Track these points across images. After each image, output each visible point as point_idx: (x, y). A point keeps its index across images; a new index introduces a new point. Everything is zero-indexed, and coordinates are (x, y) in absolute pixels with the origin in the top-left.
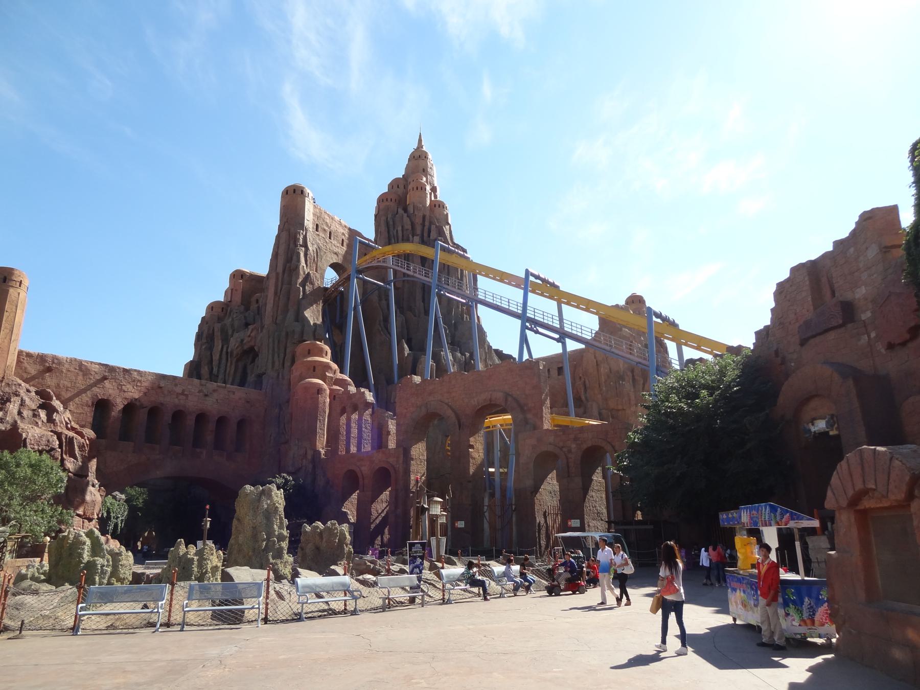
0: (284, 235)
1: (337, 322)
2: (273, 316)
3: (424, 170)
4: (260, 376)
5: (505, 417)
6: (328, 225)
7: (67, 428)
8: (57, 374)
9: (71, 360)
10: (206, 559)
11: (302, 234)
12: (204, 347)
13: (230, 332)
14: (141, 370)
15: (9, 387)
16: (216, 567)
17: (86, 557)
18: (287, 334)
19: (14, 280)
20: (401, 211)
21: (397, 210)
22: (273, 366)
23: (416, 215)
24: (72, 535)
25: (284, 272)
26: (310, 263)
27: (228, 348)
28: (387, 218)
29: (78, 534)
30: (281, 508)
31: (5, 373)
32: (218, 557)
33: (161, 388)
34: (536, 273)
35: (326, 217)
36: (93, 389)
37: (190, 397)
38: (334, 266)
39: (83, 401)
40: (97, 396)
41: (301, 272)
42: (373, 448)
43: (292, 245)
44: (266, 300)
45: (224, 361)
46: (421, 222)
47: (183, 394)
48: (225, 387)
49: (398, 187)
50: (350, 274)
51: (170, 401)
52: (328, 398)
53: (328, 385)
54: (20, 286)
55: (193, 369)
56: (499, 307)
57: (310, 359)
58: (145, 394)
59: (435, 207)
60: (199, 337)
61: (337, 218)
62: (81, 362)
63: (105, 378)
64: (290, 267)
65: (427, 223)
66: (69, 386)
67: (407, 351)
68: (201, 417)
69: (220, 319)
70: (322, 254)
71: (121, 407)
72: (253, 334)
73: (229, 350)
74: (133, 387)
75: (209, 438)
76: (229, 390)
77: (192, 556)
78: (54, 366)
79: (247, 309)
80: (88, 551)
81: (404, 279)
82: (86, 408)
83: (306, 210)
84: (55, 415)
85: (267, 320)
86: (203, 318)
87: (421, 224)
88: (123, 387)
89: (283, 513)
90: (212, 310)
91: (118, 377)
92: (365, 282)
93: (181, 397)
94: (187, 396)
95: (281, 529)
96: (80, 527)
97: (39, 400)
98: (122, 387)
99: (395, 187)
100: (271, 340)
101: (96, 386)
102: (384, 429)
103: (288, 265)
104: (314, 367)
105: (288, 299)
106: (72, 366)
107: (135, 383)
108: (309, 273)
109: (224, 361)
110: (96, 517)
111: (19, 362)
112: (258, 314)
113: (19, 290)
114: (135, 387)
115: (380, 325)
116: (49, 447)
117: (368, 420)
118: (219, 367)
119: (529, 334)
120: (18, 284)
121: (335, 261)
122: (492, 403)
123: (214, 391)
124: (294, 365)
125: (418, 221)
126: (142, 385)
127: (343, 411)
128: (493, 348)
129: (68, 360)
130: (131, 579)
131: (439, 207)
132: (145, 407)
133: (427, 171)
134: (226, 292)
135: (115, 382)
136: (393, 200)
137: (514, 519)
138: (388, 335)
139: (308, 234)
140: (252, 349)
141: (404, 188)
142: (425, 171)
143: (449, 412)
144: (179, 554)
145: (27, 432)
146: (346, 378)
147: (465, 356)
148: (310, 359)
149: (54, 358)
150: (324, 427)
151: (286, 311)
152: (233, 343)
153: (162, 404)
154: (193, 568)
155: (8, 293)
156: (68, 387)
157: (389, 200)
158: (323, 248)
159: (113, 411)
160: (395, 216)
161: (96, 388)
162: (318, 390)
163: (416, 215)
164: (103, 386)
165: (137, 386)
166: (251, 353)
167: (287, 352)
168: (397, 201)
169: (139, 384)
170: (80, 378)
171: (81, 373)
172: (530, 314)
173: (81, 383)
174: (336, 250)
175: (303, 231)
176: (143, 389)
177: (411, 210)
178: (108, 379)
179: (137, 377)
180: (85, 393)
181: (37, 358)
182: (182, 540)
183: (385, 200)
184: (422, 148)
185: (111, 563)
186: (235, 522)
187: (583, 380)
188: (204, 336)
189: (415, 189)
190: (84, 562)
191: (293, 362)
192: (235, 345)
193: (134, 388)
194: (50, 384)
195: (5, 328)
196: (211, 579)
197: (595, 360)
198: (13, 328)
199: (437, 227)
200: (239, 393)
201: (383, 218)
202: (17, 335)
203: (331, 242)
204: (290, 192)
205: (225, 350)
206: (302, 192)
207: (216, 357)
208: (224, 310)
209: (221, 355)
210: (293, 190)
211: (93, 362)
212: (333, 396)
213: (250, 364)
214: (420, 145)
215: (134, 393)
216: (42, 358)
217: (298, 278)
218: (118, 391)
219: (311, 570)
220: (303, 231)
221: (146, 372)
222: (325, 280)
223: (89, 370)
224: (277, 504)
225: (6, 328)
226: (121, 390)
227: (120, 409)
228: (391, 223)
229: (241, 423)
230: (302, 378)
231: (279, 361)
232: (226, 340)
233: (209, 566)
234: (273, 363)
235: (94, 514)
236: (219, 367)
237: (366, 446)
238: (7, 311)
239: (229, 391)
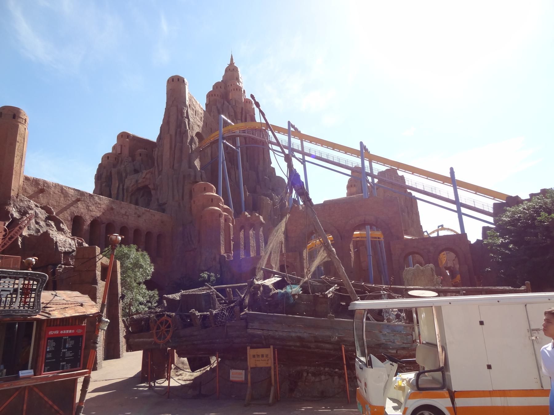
6: (194, 106)
8: (47, 195)
9: (56, 184)
11: (186, 109)
12: (104, 185)
13: (124, 175)
15: (22, 202)
19: (22, 118)
20: (226, 102)
23: (237, 107)
25: (176, 134)
27: (123, 186)
31: (19, 191)
35: (194, 100)
36: (71, 208)
39: (65, 217)
40: (73, 213)
43: (180, 117)
46: (241, 111)
47: (125, 214)
49: (221, 88)
54: (25, 123)
57: (207, 194)
58: (103, 213)
61: (198, 103)
62: (62, 187)
63: (78, 200)
64: (180, 131)
65: (244, 113)
69: (114, 166)
71: (89, 222)
73: (125, 187)
74: (96, 208)
79: (133, 160)
82: (67, 222)
88: (90, 207)
91: (86, 200)
92: (228, 146)
94: (128, 216)
97: (46, 214)
98: (89, 208)
101: (72, 206)
104: (212, 199)
106: (56, 189)
107: (97, 206)
114: (97, 208)
116: (71, 249)
120: (24, 121)
121: (198, 131)
123: (143, 213)
126: (101, 207)
127: (242, 227)
129: (54, 184)
131: (249, 103)
132: (104, 223)
133: (239, 80)
141: (225, 89)
145: (56, 237)
148: (207, 194)
149: (45, 182)
155: (18, 127)
156: (55, 206)
159: (85, 225)
161: (73, 207)
162: (220, 214)
163: (237, 107)
164: (77, 206)
165: (98, 207)
170: (62, 199)
171: (62, 195)
173: (63, 203)
175: (186, 107)
179: (98, 201)
180: (66, 210)
181: (33, 182)
183: (213, 95)
189: (235, 90)
193: (96, 209)
194: (42, 202)
195: (17, 155)
198: (22, 156)
205: (121, 187)
210: (172, 80)
211: (70, 187)
214: (232, 63)
216: (36, 182)
217: (187, 139)
218: (86, 210)
223: (68, 193)
225: (18, 155)
226: (89, 210)
227: (88, 224)
229: (159, 236)
232: (121, 180)
239: (151, 214)
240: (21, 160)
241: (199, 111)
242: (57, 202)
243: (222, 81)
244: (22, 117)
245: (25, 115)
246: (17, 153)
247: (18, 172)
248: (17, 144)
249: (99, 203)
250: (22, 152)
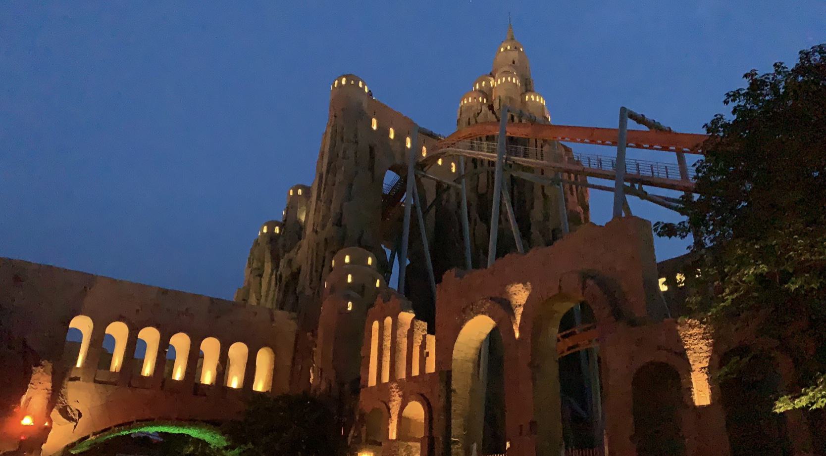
100: (310, 252)
172: (631, 170)
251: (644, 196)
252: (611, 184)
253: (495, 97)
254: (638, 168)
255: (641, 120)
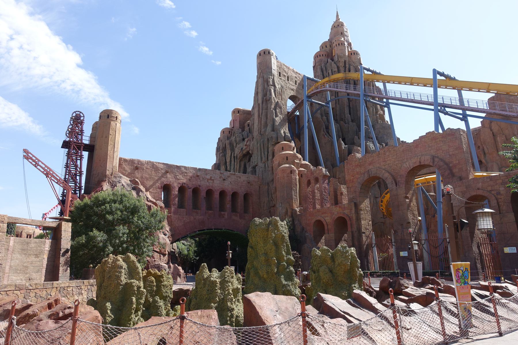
0: (261, 80)
1: (297, 133)
2: (258, 130)
3: (342, 33)
4: (254, 168)
5: (426, 177)
6: (286, 72)
7: (148, 201)
9: (148, 162)
10: (227, 282)
11: (272, 78)
12: (221, 155)
14: (186, 166)
16: (238, 289)
17: (124, 279)
18: (268, 139)
20: (329, 60)
21: (327, 60)
22: (261, 160)
24: (111, 260)
26: (278, 96)
28: (321, 67)
29: (116, 259)
30: (287, 236)
32: (237, 280)
33: (198, 176)
34: (441, 71)
35: (285, 67)
37: (215, 181)
38: (292, 98)
41: (273, 101)
42: (332, 205)
43: (266, 86)
44: (254, 121)
45: (233, 162)
46: (343, 65)
47: (211, 179)
48: (235, 174)
49: (326, 47)
50: (303, 100)
51: (204, 185)
52: (297, 176)
53: (298, 168)
54: (116, 120)
55: (217, 166)
56: (413, 100)
59: (351, 54)
60: (218, 149)
61: (291, 68)
65: (347, 66)
66: (148, 177)
67: (343, 146)
68: (222, 193)
70: (284, 90)
72: (248, 144)
73: (235, 155)
75: (228, 206)
76: (237, 176)
77: (215, 279)
78: (139, 166)
80: (125, 274)
81: (336, 99)
82: (158, 190)
83: (272, 63)
84: (141, 193)
85: (256, 133)
86: (219, 139)
87: (344, 66)
88: (177, 176)
89: (289, 241)
90: (224, 133)
93: (210, 181)
95: (289, 255)
96: (158, 259)
99: (324, 47)
100: (259, 145)
102: (338, 192)
103: (265, 98)
105: (267, 118)
106: (149, 165)
108: (278, 102)
109: (233, 162)
110: (167, 253)
111: (120, 164)
112: (250, 132)
113: (116, 122)
115: (324, 131)
117: (326, 187)
118: (230, 166)
119: (441, 115)
120: (115, 118)
122: (422, 164)
123: (228, 177)
124: (275, 157)
125: (341, 65)
128: (401, 140)
130: (172, 297)
134: (230, 122)
135: (173, 174)
136: (324, 55)
137: (449, 249)
138: (330, 137)
139: (275, 78)
140: (248, 153)
142: (342, 34)
143: (387, 175)
144: (203, 277)
146: (307, 163)
147: (382, 145)
149: (139, 161)
150: (297, 194)
151: (266, 125)
152: (237, 151)
153: (200, 186)
154: (216, 290)
157: (321, 56)
158: (285, 87)
160: (326, 64)
166: (247, 156)
167: (269, 151)
168: (327, 56)
169: (186, 175)
170: (153, 172)
172: (440, 101)
174: (291, 89)
175: (272, 76)
176: (188, 177)
177: (336, 59)
178: (168, 172)
182: (205, 264)
183: (319, 56)
184: (339, 20)
185: (155, 284)
186: (249, 250)
187: (481, 148)
188: (221, 148)
189: (338, 45)
190: (122, 284)
191: (273, 156)
192: (238, 152)
196: (234, 300)
197: (491, 132)
199: (354, 67)
200: (244, 178)
201: (319, 67)
202: (117, 148)
203: (289, 83)
204: (262, 53)
205: (233, 155)
206: (269, 52)
207: (228, 160)
208: (230, 133)
209: (231, 158)
212: (301, 175)
213: (248, 162)
215: (183, 180)
216: (131, 162)
219: (326, 294)
220: (272, 76)
221: (189, 167)
222: (287, 107)
224: (283, 233)
228: (324, 69)
229: (246, 196)
230: (280, 165)
231: (265, 157)
232: (233, 150)
233: (231, 288)
234: (261, 158)
235: (166, 251)
236: (230, 166)
237: (326, 204)
238: (111, 135)
239: (237, 177)
240: (113, 147)
241: (293, 75)
242: (149, 175)
243: (329, 40)
244: (113, 116)
245: (116, 114)
246: (110, 142)
247: (112, 156)
248: (110, 136)
249: (186, 173)
250: (114, 142)
251: (446, 113)
252: (432, 107)
253: (335, 54)
254: (468, 103)
255: (442, 74)
